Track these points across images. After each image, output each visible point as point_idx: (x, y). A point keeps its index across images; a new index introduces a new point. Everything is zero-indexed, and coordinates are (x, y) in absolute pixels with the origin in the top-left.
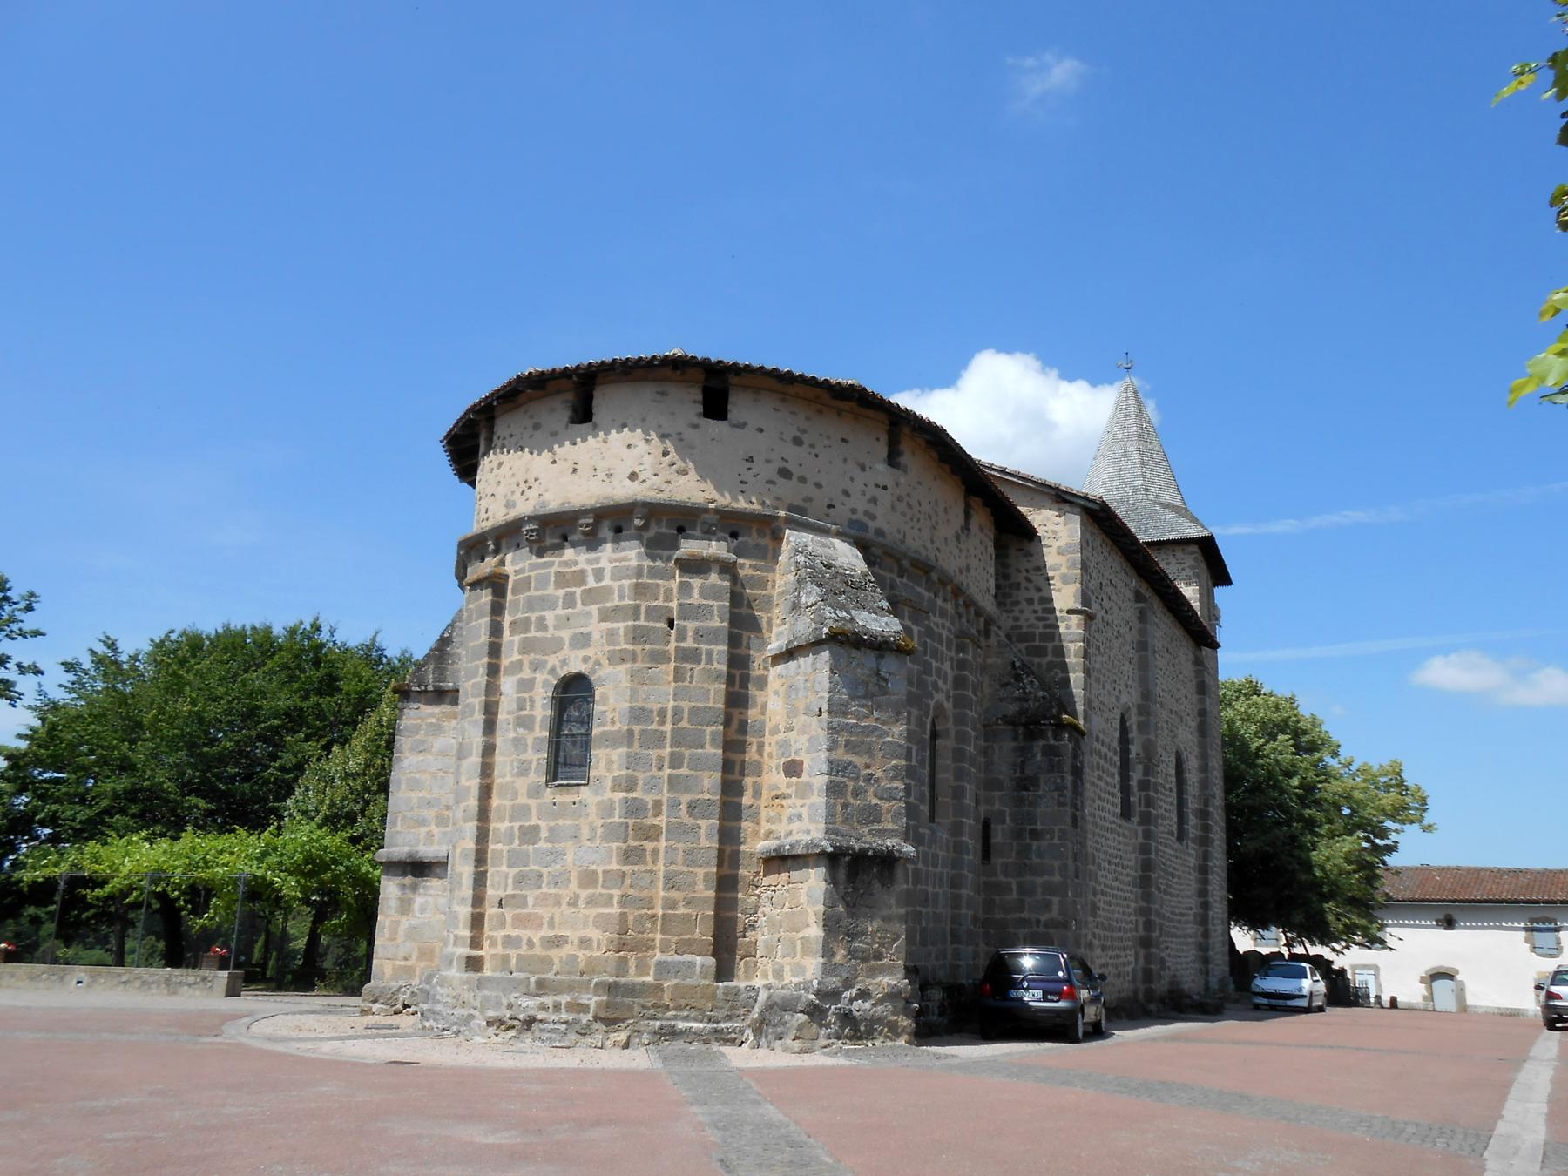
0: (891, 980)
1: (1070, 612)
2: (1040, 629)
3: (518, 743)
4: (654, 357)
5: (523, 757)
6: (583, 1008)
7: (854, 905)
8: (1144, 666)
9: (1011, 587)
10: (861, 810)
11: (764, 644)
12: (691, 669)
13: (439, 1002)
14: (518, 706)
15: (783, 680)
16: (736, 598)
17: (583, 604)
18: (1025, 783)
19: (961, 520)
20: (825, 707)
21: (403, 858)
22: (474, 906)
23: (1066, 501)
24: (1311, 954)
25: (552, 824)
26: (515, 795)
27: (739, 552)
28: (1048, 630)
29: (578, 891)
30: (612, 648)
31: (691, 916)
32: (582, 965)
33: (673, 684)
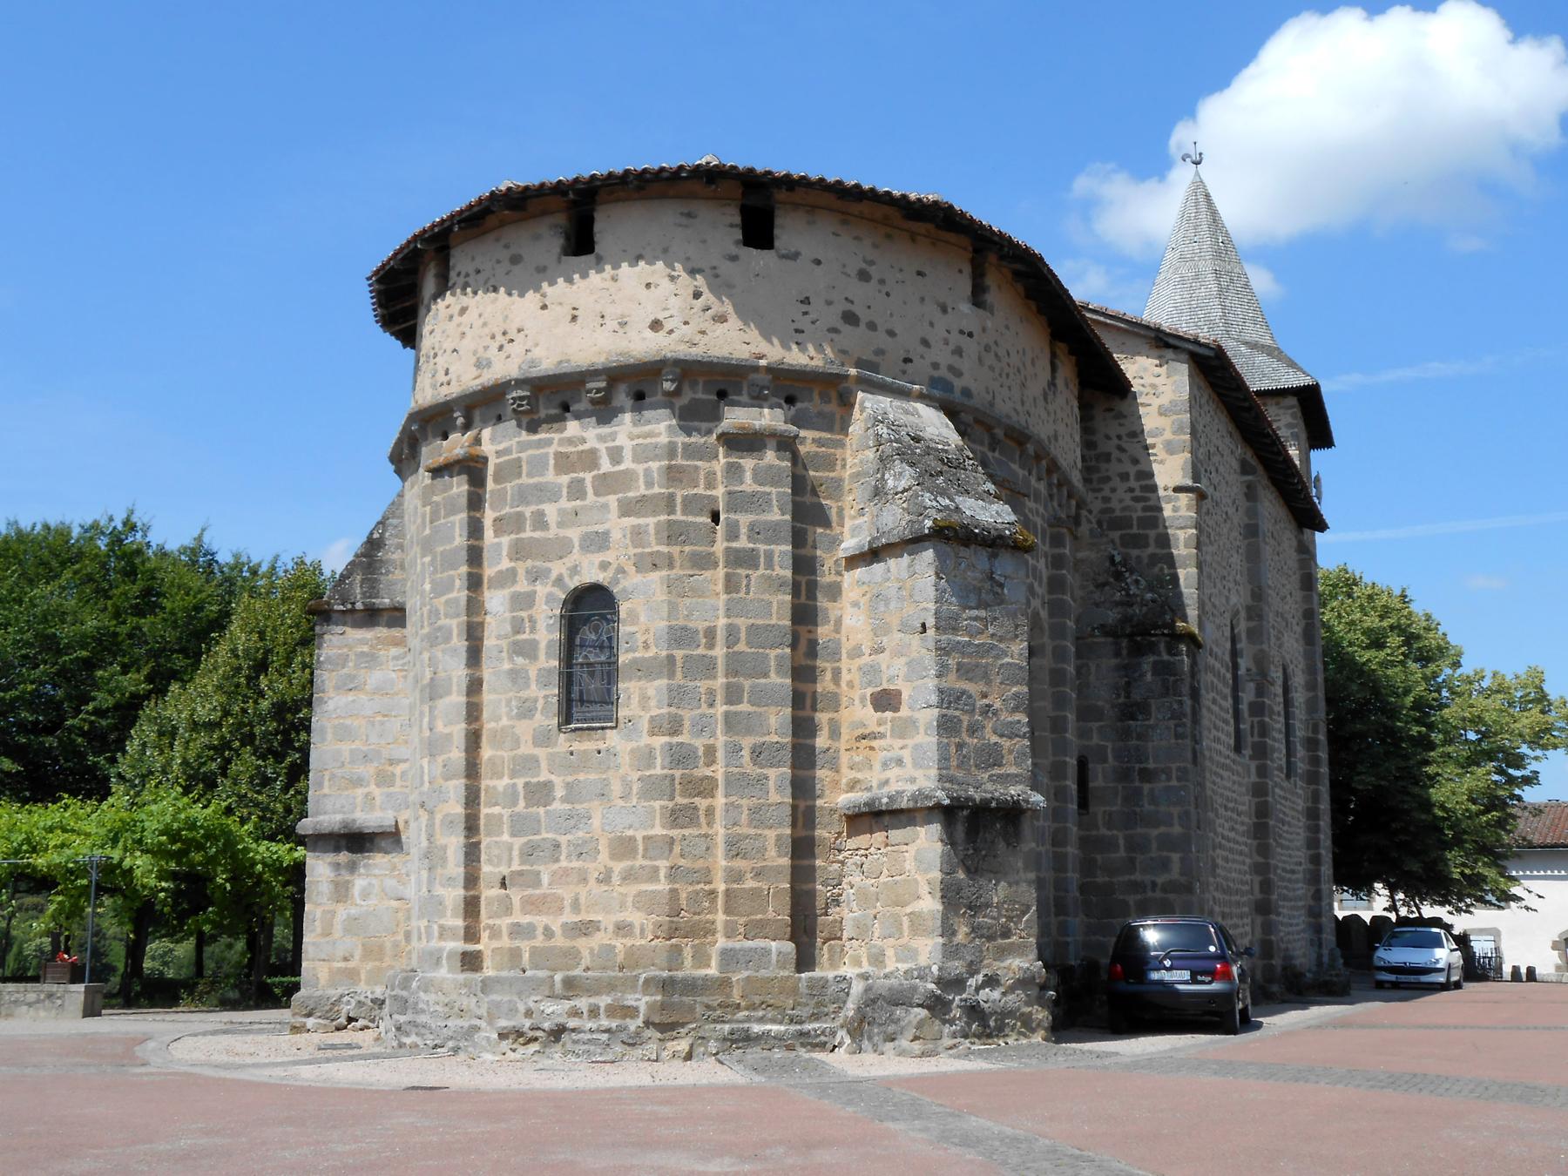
0: (1022, 963)
1: (1178, 489)
2: (1138, 512)
3: (516, 676)
4: (681, 168)
5: (525, 694)
6: (631, 1012)
7: (976, 871)
8: (1253, 555)
9: (1098, 458)
10: (979, 751)
11: (835, 542)
12: (747, 576)
13: (423, 1011)
14: (513, 627)
15: (865, 588)
16: (799, 484)
17: (597, 494)
18: (1131, 711)
19: (1047, 375)
20: (931, 622)
21: (336, 829)
22: (466, 888)
23: (1168, 346)
24: (1426, 916)
25: (570, 779)
26: (517, 743)
27: (796, 421)
28: (1148, 514)
29: (611, 864)
30: (640, 550)
31: (762, 891)
32: (620, 958)
33: (724, 597)
